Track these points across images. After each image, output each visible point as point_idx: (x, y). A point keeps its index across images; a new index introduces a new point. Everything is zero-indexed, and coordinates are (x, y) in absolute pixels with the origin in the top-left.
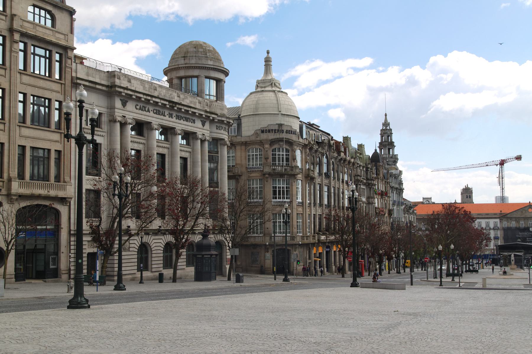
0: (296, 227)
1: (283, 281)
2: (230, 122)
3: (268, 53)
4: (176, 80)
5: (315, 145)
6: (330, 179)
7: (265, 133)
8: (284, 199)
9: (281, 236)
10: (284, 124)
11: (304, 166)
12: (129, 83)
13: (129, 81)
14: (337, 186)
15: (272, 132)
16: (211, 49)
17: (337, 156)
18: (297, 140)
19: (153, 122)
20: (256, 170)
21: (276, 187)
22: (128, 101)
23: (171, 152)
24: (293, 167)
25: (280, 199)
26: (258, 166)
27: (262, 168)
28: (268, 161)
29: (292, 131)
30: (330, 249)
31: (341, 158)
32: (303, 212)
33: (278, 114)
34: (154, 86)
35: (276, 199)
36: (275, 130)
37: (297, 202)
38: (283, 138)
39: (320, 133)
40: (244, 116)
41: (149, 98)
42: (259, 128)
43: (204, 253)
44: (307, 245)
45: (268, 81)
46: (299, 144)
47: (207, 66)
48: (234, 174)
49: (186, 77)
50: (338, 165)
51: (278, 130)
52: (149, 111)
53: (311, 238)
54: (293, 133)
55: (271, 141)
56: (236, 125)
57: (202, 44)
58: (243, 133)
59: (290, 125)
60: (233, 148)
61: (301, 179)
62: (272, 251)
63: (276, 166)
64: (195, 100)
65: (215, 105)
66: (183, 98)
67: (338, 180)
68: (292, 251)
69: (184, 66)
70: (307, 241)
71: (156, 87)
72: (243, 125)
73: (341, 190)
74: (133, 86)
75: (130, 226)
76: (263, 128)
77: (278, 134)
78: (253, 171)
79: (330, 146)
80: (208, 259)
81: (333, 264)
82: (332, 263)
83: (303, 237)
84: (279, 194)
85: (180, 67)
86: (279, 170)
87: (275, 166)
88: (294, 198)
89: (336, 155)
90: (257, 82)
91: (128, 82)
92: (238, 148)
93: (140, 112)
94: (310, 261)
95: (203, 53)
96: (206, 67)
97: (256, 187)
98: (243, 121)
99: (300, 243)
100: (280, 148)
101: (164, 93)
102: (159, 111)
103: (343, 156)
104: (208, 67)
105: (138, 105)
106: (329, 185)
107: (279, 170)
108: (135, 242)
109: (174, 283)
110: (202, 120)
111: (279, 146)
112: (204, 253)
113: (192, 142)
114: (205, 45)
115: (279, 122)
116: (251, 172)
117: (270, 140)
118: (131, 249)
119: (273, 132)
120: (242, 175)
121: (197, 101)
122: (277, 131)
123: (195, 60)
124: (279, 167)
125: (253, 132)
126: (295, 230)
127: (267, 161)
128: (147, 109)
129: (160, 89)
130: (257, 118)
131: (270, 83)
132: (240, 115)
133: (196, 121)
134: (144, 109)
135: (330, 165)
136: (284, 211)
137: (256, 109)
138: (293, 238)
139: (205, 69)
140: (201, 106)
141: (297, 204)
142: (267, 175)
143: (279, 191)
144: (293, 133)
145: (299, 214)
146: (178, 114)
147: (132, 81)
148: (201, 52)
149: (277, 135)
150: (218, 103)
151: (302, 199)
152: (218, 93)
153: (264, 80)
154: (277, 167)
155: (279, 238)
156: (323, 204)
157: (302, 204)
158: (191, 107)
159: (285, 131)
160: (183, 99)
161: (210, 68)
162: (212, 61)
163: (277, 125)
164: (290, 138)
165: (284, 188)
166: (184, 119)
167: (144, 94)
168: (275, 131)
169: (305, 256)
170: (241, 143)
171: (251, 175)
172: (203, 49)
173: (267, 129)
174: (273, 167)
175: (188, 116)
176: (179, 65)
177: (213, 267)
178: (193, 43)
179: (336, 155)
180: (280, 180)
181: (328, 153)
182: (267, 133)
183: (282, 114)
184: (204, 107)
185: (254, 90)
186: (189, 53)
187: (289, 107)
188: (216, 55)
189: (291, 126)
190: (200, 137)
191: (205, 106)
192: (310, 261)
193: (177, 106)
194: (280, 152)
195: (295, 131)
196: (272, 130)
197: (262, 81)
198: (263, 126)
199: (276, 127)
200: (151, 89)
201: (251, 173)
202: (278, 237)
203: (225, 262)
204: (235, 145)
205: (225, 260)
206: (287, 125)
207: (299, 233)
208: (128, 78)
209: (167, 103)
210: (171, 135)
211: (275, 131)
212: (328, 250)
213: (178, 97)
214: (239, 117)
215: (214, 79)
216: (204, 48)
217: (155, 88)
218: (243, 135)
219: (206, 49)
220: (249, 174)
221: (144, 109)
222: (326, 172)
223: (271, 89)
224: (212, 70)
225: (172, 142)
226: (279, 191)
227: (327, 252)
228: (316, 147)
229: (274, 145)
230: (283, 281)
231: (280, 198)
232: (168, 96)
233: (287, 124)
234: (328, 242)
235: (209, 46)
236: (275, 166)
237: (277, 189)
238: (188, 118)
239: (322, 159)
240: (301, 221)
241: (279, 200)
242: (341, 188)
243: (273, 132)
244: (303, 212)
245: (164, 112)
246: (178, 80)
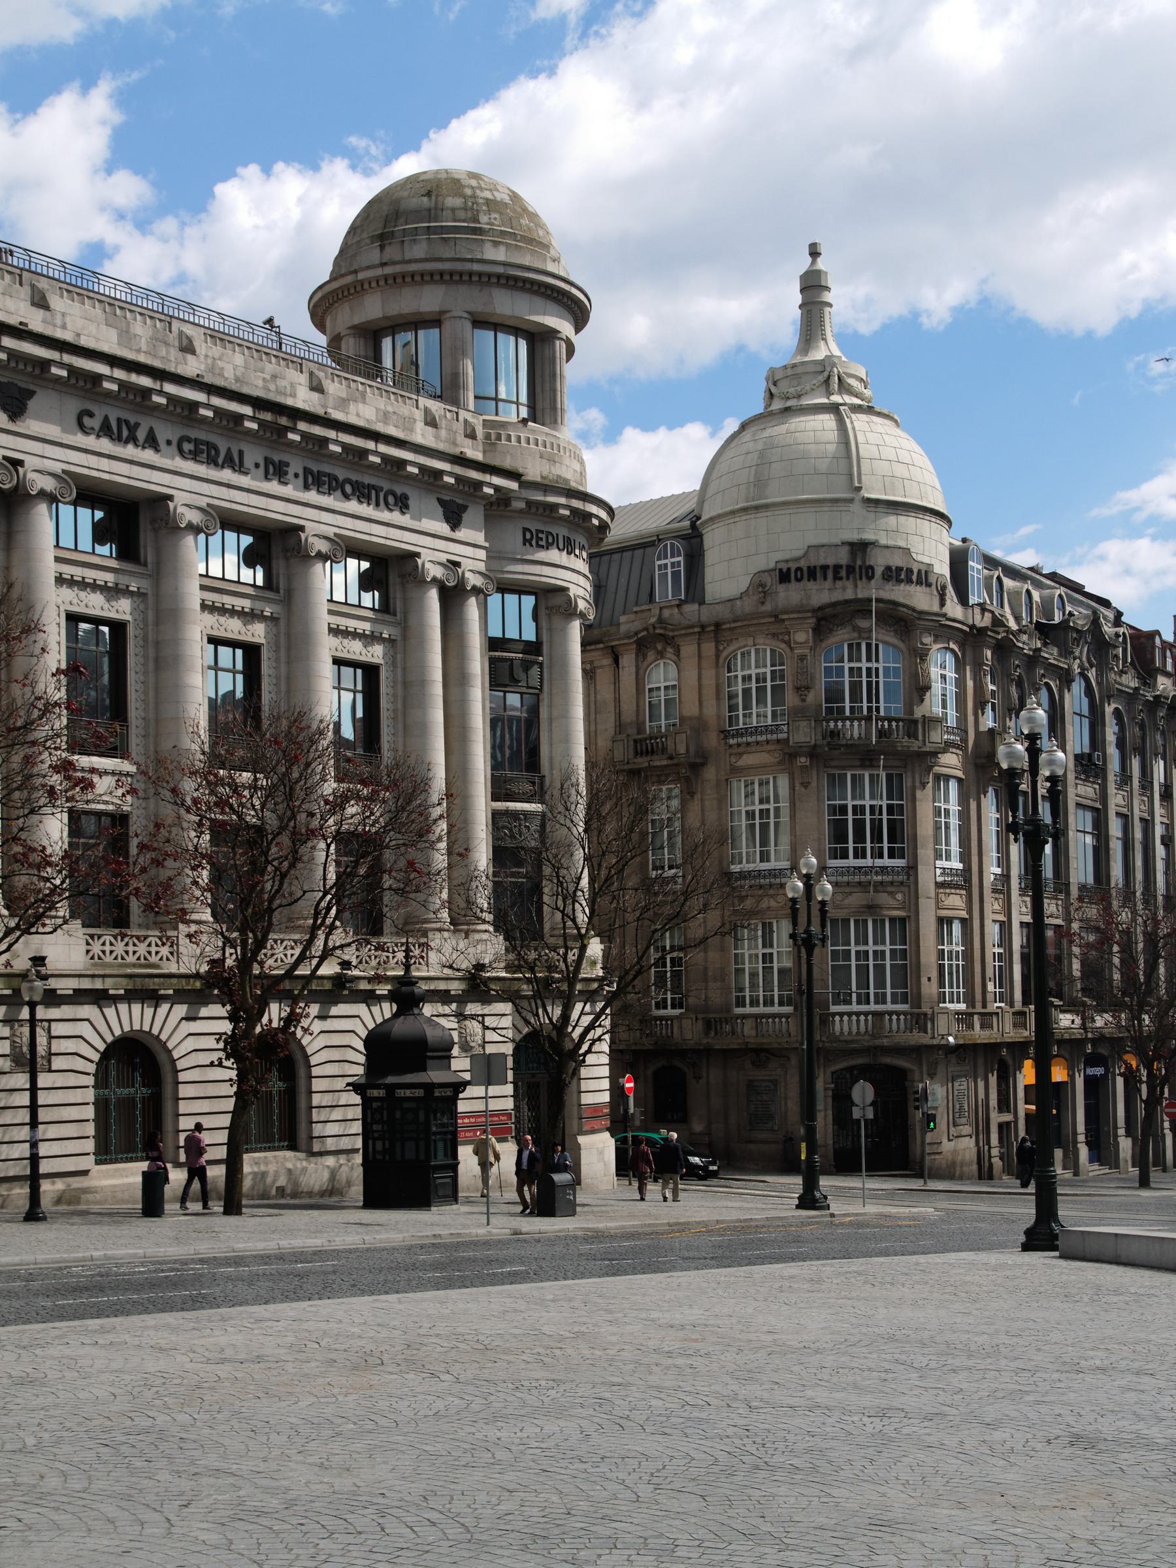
0: (934, 975)
1: (798, 1207)
2: (590, 515)
3: (814, 253)
4: (351, 340)
5: (1025, 637)
6: (1105, 779)
7: (794, 585)
8: (881, 856)
9: (866, 1014)
10: (874, 544)
11: (971, 718)
12: (42, 311)
13: (40, 302)
14: (1137, 813)
15: (825, 579)
16: (501, 196)
17: (1136, 689)
18: (936, 608)
19: (180, 498)
20: (759, 738)
21: (846, 806)
22: (31, 394)
23: (288, 635)
24: (915, 722)
25: (864, 857)
26: (769, 722)
27: (785, 728)
28: (811, 698)
29: (910, 571)
30: (1107, 1071)
31: (1156, 697)
32: (970, 912)
33: (851, 501)
34: (181, 333)
35: (847, 857)
36: (837, 568)
37: (938, 871)
38: (870, 600)
39: (1058, 592)
40: (712, 519)
41: (145, 381)
42: (772, 565)
43: (391, 1080)
44: (991, 1049)
45: (811, 369)
46: (943, 630)
47: (476, 267)
48: (671, 758)
49: (393, 326)
50: (1142, 727)
51: (848, 567)
52: (152, 442)
53: (1008, 1020)
54: (914, 578)
55: (820, 614)
56: (681, 559)
57: (463, 177)
58: (709, 589)
59: (902, 544)
60: (668, 655)
61: (960, 774)
62: (829, 1074)
63: (844, 719)
64: (406, 409)
65: (519, 438)
66: (344, 395)
67: (1143, 787)
68: (917, 1076)
69: (379, 272)
70: (987, 1033)
71: (190, 340)
72: (712, 557)
73: (1159, 831)
74: (64, 327)
75: (43, 959)
76: (787, 561)
77: (849, 584)
78: (748, 744)
79: (1101, 647)
80: (413, 1105)
81: (1121, 1132)
82: (1116, 1128)
83: (964, 1018)
84: (860, 837)
85: (362, 283)
86: (856, 735)
87: (836, 721)
88: (925, 852)
89: (1130, 681)
90: (767, 379)
91: (33, 304)
92: (688, 649)
93: (105, 445)
94: (1007, 1117)
95: (461, 214)
96: (471, 274)
97: (761, 811)
98: (712, 539)
99: (951, 1039)
100: (859, 645)
101: (235, 367)
102: (212, 446)
103: (1165, 689)
104: (480, 274)
105: (91, 415)
106: (1098, 805)
107: (856, 735)
108: (85, 1029)
109: (233, 1220)
110: (447, 498)
111: (856, 635)
112: (391, 1080)
113: (399, 595)
114: (474, 183)
115: (854, 536)
116: (741, 750)
117: (814, 611)
118: (57, 1063)
119: (830, 574)
120: (703, 765)
121: (419, 415)
122: (843, 573)
123: (424, 245)
124: (856, 723)
125: (744, 583)
126: (930, 989)
127: (804, 700)
128: (141, 434)
129: (217, 350)
130: (761, 522)
131: (821, 378)
132: (699, 518)
133: (411, 502)
134: (125, 433)
135: (1104, 724)
136: (795, 889)
137: (760, 483)
138: (920, 1020)
139: (470, 281)
140: (437, 437)
141: (940, 879)
142: (803, 760)
143: (859, 826)
144: (914, 578)
145: (950, 921)
146: (315, 467)
147: (58, 303)
148: (453, 210)
149: (844, 589)
150: (533, 431)
151: (965, 857)
152: (538, 390)
153: (794, 366)
154: (848, 723)
155: (858, 1021)
156: (1068, 885)
157: (965, 881)
158: (377, 436)
159: (879, 571)
160: (343, 403)
161: (489, 275)
162: (502, 249)
163: (846, 548)
164: (901, 600)
165: (863, 813)
166: (348, 489)
167: (113, 361)
168: (836, 572)
169: (981, 1095)
170: (696, 630)
171: (740, 763)
172: (464, 197)
173: (803, 564)
174: (828, 721)
175: (367, 480)
176: (356, 272)
177: (440, 1145)
178: (421, 178)
179: (1134, 684)
180: (862, 777)
181: (1092, 674)
182: (802, 583)
183: (869, 501)
184: (455, 444)
185: (759, 408)
186: (402, 220)
187: (900, 470)
188: (525, 221)
189: (907, 551)
190: (434, 571)
191: (460, 438)
192: (1007, 1117)
193: (302, 426)
194: (859, 660)
195: (923, 568)
196: (825, 568)
197: (789, 372)
198: (787, 556)
199: (843, 557)
200: (166, 344)
201: (741, 755)
202: (854, 1018)
203: (575, 1122)
204: (678, 641)
205: (575, 1115)
206: (887, 547)
207: (952, 1001)
208: (33, 286)
209: (247, 410)
210: (287, 559)
211: (836, 572)
212: (1099, 1071)
213: (312, 389)
214: (693, 525)
215: (517, 330)
216: (468, 192)
217: (185, 342)
218: (708, 598)
219: (474, 196)
220: (733, 760)
221: (125, 433)
222: (1087, 750)
223: (825, 401)
224: (498, 284)
225: (289, 593)
226: (859, 826)
227: (1089, 1082)
228: (1028, 643)
229: (831, 631)
230: (798, 1207)
231: (860, 854)
232: (260, 383)
233: (891, 543)
234: (1094, 1041)
235: (494, 188)
236: (836, 721)
237: (850, 817)
238: (371, 487)
239: (1062, 698)
240: (960, 948)
241: (860, 862)
242: (1158, 819)
243: (830, 574)
244: (970, 912)
245: (241, 453)
246: (362, 342)
